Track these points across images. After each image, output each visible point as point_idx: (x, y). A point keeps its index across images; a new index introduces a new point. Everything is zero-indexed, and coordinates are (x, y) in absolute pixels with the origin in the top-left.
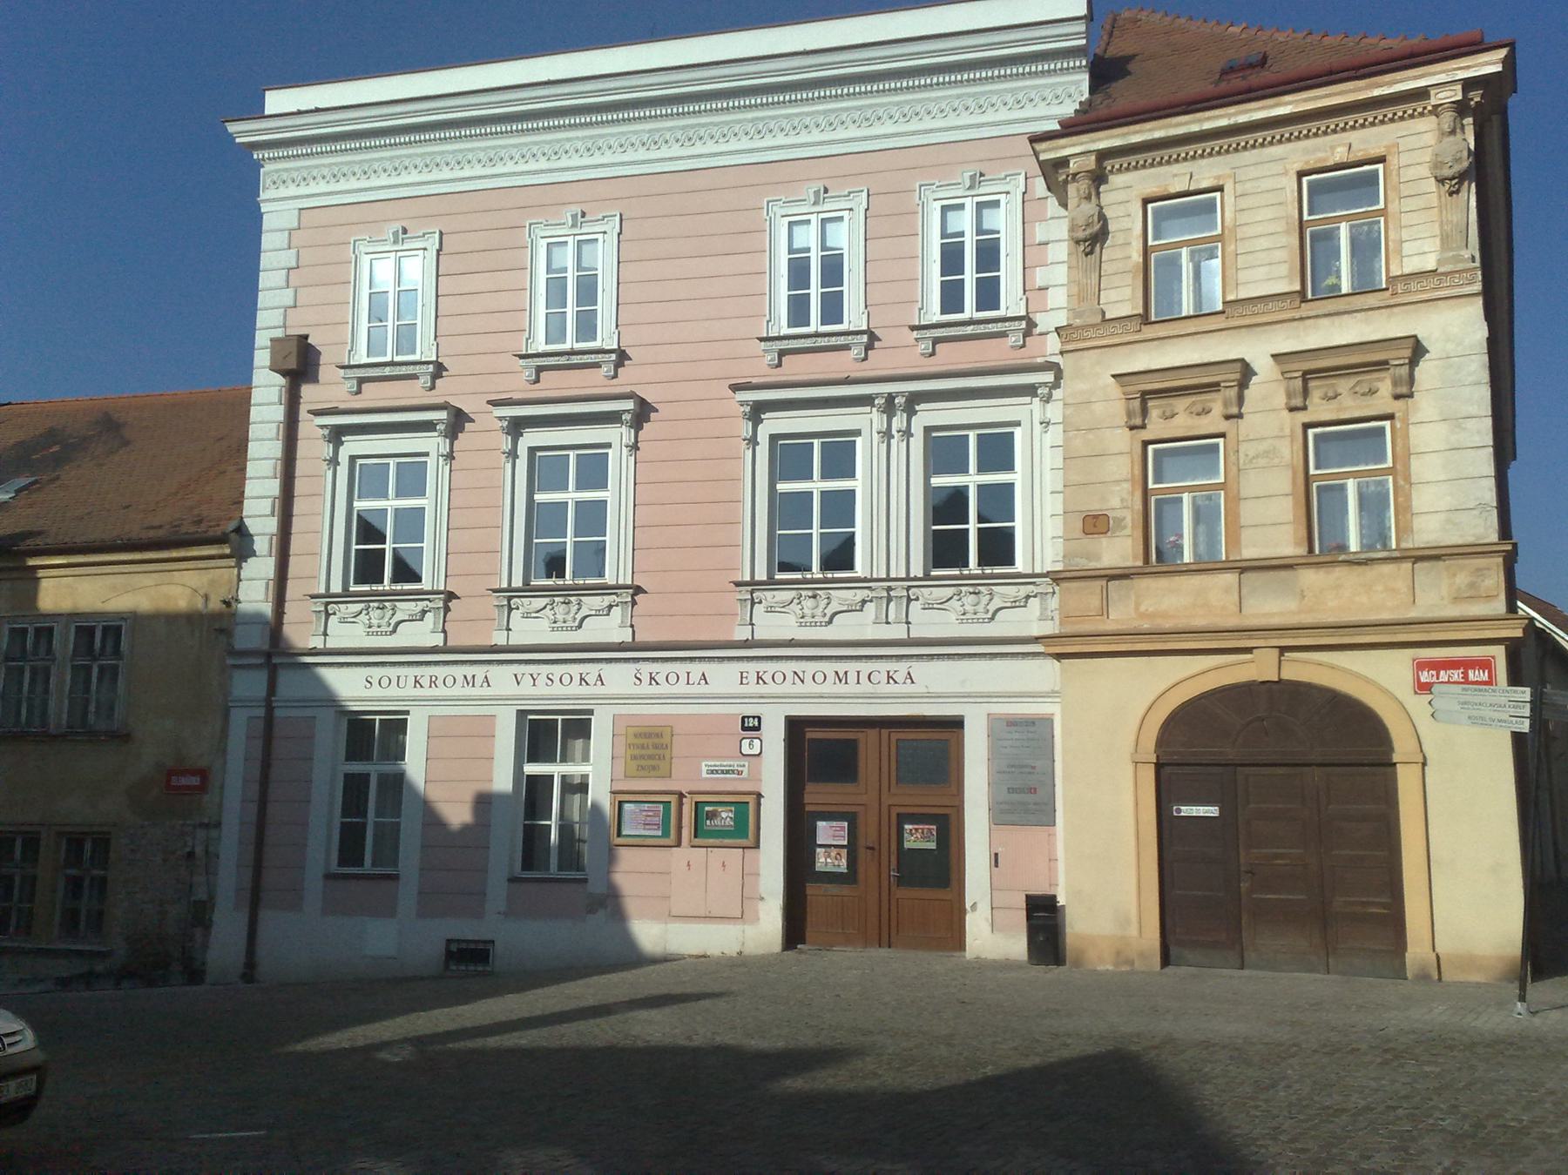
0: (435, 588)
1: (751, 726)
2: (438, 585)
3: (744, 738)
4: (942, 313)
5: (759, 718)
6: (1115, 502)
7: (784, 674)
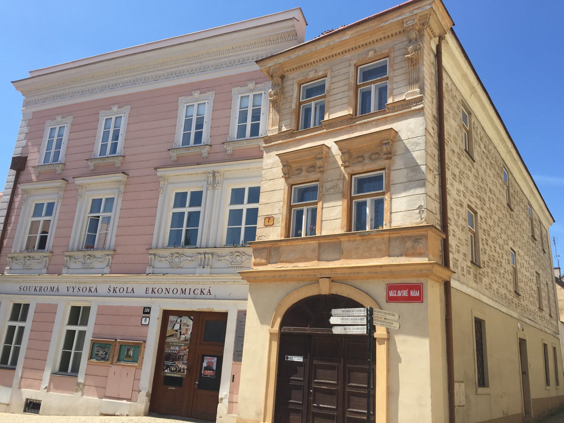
1: (147, 311)
3: (143, 317)
5: (150, 308)
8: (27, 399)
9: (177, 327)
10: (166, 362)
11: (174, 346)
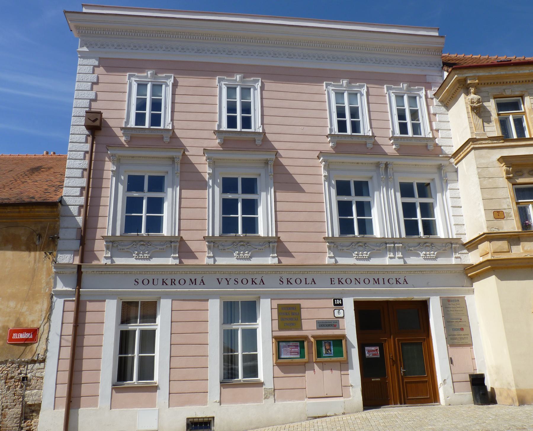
3: (335, 309)
6: (505, 206)
8: (188, 419)
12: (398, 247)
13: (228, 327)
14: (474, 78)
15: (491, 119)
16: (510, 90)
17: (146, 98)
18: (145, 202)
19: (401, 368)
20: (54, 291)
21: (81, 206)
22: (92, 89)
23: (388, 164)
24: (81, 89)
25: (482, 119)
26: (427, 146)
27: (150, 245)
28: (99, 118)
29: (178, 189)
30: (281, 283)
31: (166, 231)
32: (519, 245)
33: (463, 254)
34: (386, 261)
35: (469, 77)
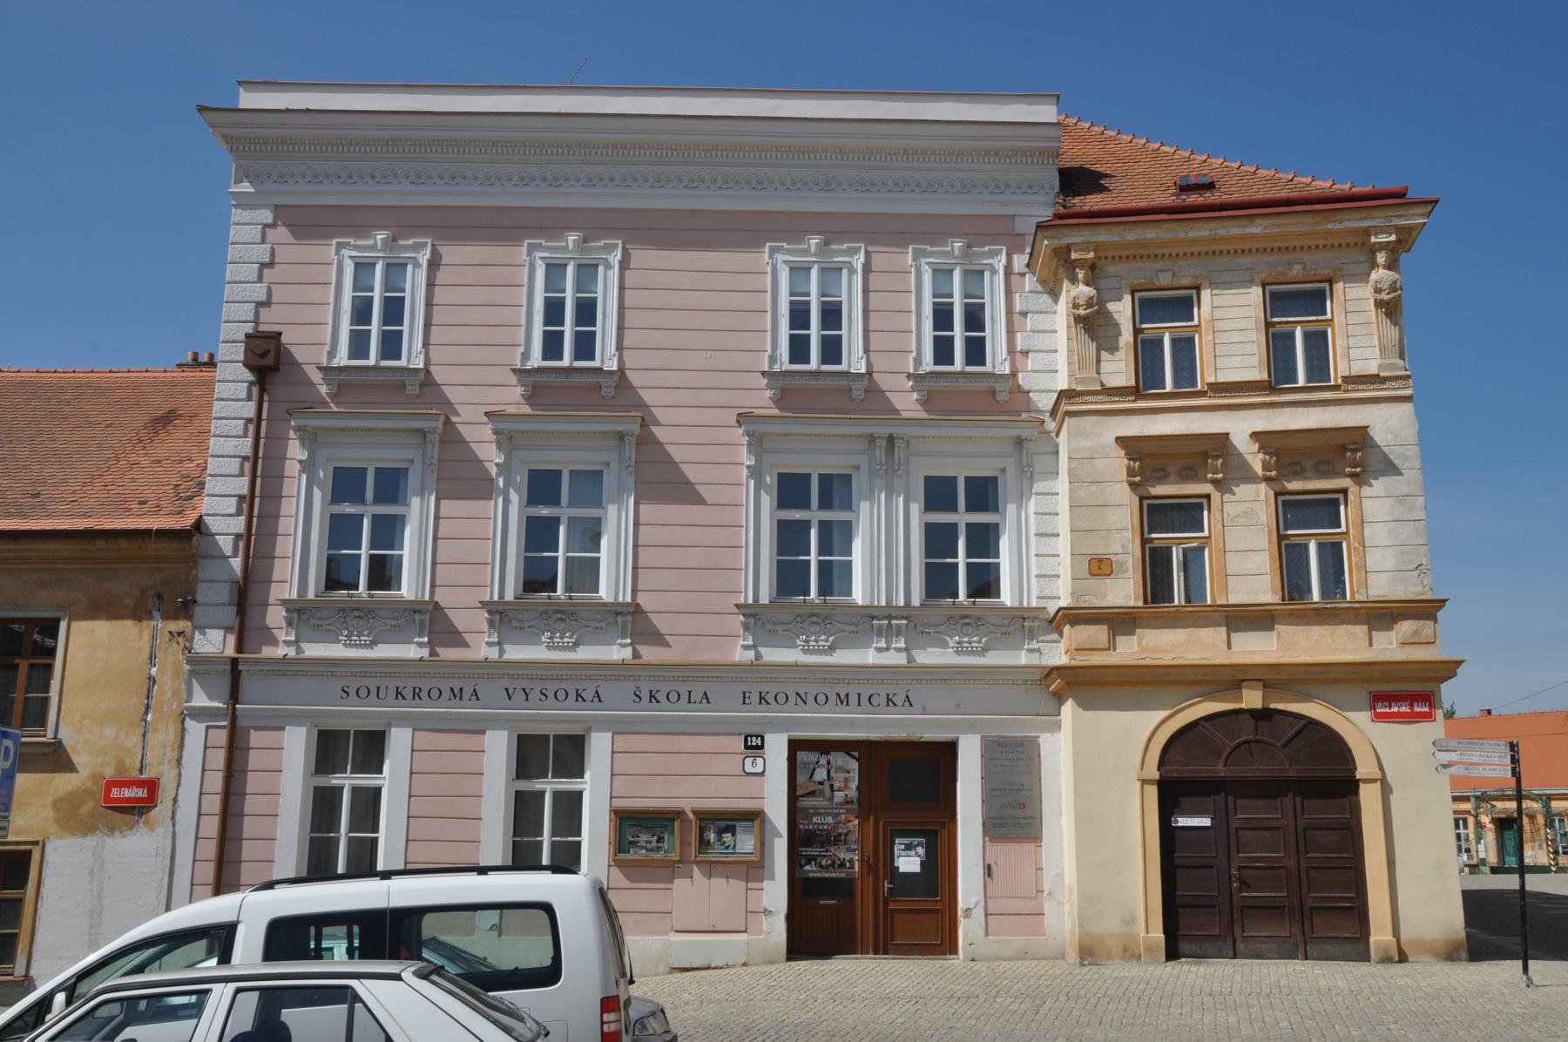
0: (621, 599)
2: (878, 601)
3: (747, 757)
4: (350, 358)
6: (1117, 548)
7: (678, 694)
9: (821, 775)
10: (804, 849)
11: (820, 814)
12: (899, 626)
13: (524, 785)
14: (1085, 247)
15: (1118, 344)
16: (1171, 273)
17: (372, 297)
18: (366, 524)
19: (886, 882)
20: (187, 708)
21: (238, 536)
22: (260, 279)
23: (894, 439)
24: (237, 279)
25: (1097, 343)
26: (994, 392)
27: (373, 618)
28: (272, 349)
29: (433, 498)
30: (637, 699)
31: (407, 589)
32: (1132, 634)
33: (1048, 642)
34: (869, 656)
35: (1075, 244)
